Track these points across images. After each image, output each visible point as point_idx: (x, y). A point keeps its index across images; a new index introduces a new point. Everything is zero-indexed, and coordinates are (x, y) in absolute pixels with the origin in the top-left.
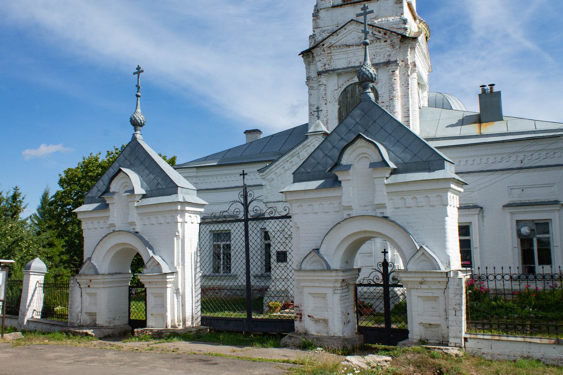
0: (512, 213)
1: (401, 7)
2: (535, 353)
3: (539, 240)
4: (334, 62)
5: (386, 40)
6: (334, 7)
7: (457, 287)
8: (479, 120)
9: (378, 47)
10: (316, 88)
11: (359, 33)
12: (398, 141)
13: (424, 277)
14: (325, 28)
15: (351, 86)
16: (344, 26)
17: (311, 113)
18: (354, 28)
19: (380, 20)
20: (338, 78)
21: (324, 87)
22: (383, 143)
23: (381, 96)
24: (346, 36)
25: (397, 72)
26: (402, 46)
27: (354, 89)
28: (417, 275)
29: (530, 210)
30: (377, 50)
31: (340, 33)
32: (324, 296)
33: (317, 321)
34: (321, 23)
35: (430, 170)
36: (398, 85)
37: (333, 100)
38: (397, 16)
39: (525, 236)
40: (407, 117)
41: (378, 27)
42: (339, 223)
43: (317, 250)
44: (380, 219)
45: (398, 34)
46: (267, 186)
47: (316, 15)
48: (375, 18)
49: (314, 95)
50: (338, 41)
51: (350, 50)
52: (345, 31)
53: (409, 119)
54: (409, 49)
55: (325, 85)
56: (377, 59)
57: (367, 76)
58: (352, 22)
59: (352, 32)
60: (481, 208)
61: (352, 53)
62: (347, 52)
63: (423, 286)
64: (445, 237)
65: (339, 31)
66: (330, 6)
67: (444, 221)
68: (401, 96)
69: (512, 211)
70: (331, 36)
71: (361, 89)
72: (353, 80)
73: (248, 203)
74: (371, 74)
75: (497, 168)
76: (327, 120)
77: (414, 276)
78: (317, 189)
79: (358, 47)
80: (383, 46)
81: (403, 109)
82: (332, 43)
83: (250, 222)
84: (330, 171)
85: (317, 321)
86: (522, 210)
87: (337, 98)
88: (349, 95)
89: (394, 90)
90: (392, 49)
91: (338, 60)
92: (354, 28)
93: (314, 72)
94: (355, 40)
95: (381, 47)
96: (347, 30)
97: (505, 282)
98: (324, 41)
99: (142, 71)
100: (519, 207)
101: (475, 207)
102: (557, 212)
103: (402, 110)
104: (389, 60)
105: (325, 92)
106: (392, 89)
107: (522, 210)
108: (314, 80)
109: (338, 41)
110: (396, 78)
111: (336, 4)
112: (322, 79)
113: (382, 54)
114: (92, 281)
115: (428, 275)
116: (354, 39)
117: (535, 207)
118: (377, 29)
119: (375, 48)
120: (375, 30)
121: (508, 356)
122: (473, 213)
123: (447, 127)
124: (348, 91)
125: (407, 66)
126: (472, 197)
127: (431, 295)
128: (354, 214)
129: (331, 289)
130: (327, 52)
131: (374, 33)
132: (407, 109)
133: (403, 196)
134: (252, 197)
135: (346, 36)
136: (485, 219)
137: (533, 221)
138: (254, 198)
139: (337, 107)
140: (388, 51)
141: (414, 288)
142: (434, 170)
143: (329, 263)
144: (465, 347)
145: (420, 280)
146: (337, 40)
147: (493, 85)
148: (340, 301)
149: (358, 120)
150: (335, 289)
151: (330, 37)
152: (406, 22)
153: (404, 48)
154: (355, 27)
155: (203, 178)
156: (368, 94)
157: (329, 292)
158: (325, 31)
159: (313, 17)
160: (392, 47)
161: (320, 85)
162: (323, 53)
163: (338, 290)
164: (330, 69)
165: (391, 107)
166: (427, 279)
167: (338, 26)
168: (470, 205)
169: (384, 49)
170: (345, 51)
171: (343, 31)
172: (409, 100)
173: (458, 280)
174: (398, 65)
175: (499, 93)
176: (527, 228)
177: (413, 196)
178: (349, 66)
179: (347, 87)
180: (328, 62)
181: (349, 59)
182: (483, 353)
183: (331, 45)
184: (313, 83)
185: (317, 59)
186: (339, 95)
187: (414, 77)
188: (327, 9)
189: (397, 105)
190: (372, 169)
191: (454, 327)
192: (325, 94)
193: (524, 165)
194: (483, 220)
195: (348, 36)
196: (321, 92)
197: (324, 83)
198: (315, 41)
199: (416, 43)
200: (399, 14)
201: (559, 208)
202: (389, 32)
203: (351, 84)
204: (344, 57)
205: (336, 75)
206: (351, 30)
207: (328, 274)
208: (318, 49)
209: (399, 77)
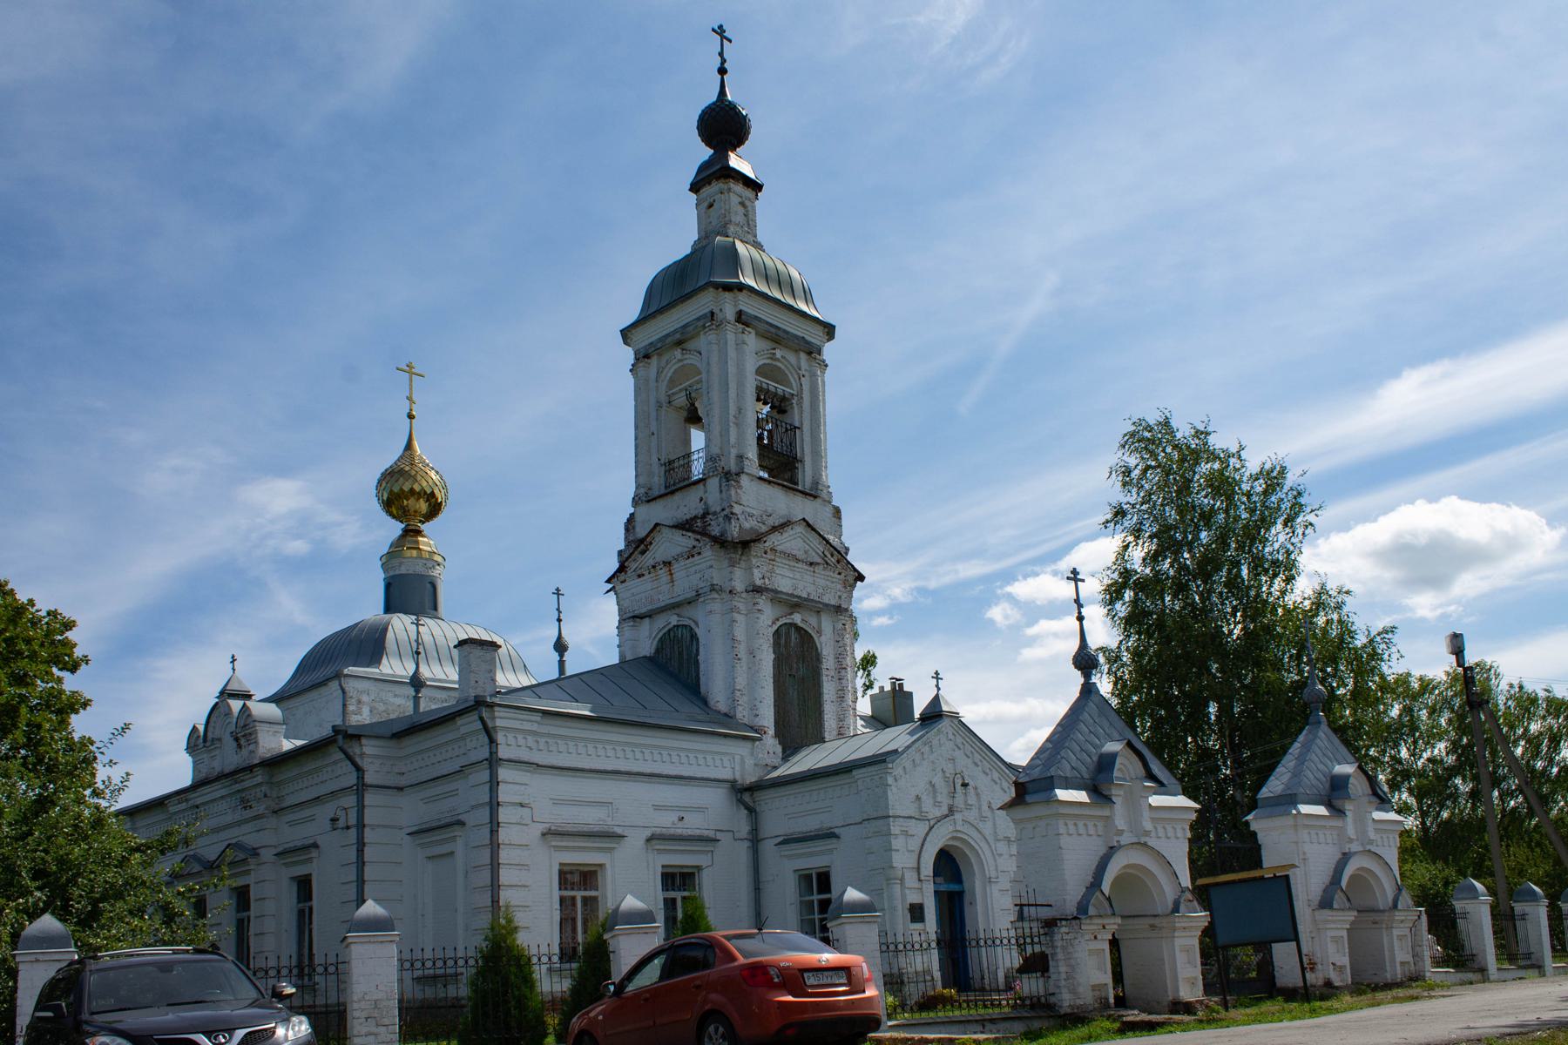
27: (789, 632)
46: (893, 787)
91: (780, 577)
97: (1012, 947)
114: (1107, 927)
154: (801, 530)
178: (795, 593)
184: (740, 602)
203: (785, 624)
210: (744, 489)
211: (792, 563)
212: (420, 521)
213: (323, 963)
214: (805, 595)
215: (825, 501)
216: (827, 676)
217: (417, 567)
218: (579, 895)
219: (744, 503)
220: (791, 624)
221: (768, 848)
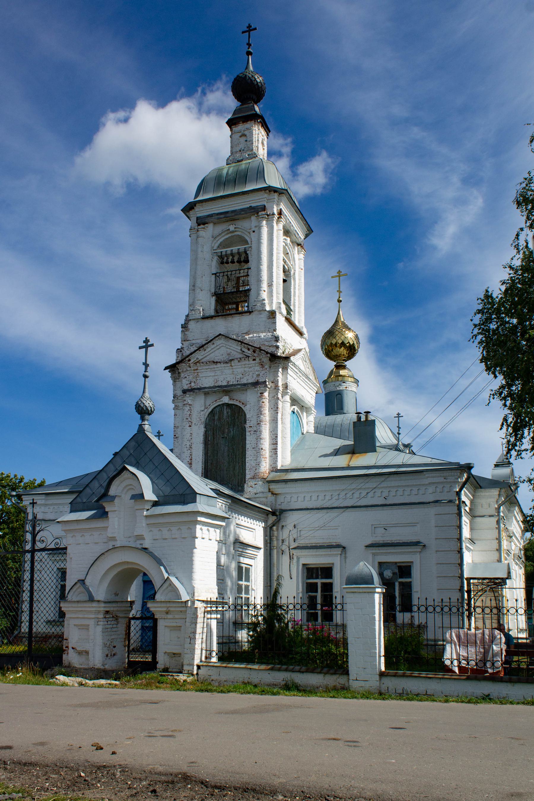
0: (374, 554)
1: (274, 323)
2: (254, 679)
3: (401, 584)
4: (200, 379)
5: (254, 358)
6: (204, 318)
7: (193, 616)
8: (352, 451)
9: (247, 366)
10: (181, 408)
11: (227, 349)
12: (162, 474)
13: (168, 607)
14: (194, 342)
15: (219, 408)
16: (212, 340)
17: (175, 436)
18: (222, 343)
19: (251, 336)
20: (205, 398)
21: (188, 408)
22: (150, 475)
23: (248, 420)
24: (215, 351)
25: (266, 394)
26: (272, 365)
27: (222, 410)
28: (163, 605)
29: (392, 551)
30: (246, 369)
31: (207, 347)
32: (86, 627)
33: (80, 653)
34: (190, 335)
35: (184, 503)
36: (267, 409)
37: (199, 422)
38: (270, 332)
39: (387, 580)
40: (275, 444)
41: (247, 344)
42: (103, 554)
43: (83, 581)
44: (139, 550)
45: (267, 353)
47: (185, 327)
48: (246, 333)
49: (179, 415)
50: (206, 357)
51: (217, 368)
52: (213, 346)
53: (277, 447)
54: (280, 370)
55: (190, 405)
56: (245, 378)
57: (142, 408)
58: (220, 336)
59: (220, 347)
60: (344, 548)
61: (220, 371)
62: (214, 369)
63: (169, 616)
64: (192, 568)
65: (207, 345)
66: (200, 317)
67: (192, 553)
68: (270, 420)
69: (374, 551)
70: (198, 351)
71: (229, 410)
72: (221, 401)
73: (37, 532)
74: (146, 406)
75: (362, 505)
76: (191, 444)
77: (160, 606)
78: (87, 519)
79: (225, 365)
80: (251, 365)
81: (272, 436)
82: (199, 359)
83: (36, 553)
84: (97, 501)
85: (80, 653)
86: (384, 551)
87: (203, 420)
88: (216, 418)
89: (261, 414)
90: (261, 369)
91: (204, 378)
92: (222, 343)
93: (179, 389)
94: (224, 356)
95: (250, 366)
96: (215, 345)
98: (191, 356)
99: (152, 345)
100: (380, 548)
101: (338, 546)
102: (418, 554)
103: (270, 437)
104: (258, 380)
105: (189, 413)
106: (259, 413)
107: (384, 551)
108: (179, 398)
109: (206, 357)
110: (264, 400)
111: (207, 315)
112: (186, 398)
113: (251, 373)
115: (172, 605)
116: (223, 355)
117: (396, 548)
118: (246, 345)
119: (243, 366)
120: (244, 347)
121: (232, 682)
122: (335, 553)
123: (320, 457)
124: (215, 412)
125: (276, 387)
126: (336, 535)
127: (175, 624)
128: (118, 544)
129: (93, 620)
130: (193, 369)
131: (244, 349)
132: (275, 435)
133: (161, 528)
134: (40, 527)
135: (215, 351)
136: (347, 560)
137: (396, 563)
138: (42, 528)
139: (202, 430)
140: (257, 371)
141: (162, 618)
142: (187, 504)
143: (93, 594)
144: (197, 674)
145: (165, 609)
146: (204, 356)
147: (370, 412)
148: (103, 632)
149: (132, 452)
150: (98, 620)
151: (196, 352)
152: (277, 339)
153: (274, 368)
154: (223, 342)
155: (52, 507)
156: (143, 426)
157: (91, 623)
158: (193, 344)
159: (182, 328)
160: (261, 366)
161: (184, 405)
162: (189, 369)
163: (101, 621)
164: (196, 387)
165: (258, 433)
166: (171, 609)
167: (207, 340)
168: (333, 544)
169: (253, 368)
170: (212, 368)
171: (211, 346)
172: (277, 425)
173: (194, 609)
174: (266, 386)
175: (373, 422)
176: (389, 571)
177: (168, 528)
178: (217, 385)
179: (215, 408)
180: (194, 380)
181: (216, 377)
182: (212, 680)
183: (198, 360)
185: (182, 375)
186: (206, 417)
187: (285, 400)
188: (197, 320)
189: (264, 431)
190: (133, 500)
191: (188, 655)
192: (190, 415)
193: (388, 502)
194: (345, 560)
195: (216, 352)
196: (186, 413)
197: (190, 403)
198: (182, 355)
199: (289, 362)
200: (271, 330)
201: (420, 550)
202: (258, 350)
203: (219, 405)
204: (211, 375)
205: (203, 394)
206: (219, 345)
207: (89, 604)
208: (184, 364)
209: (268, 400)
210: (190, 330)
211: (212, 366)
212: (344, 360)
213: (428, 614)
214: (225, 383)
215: (260, 311)
216: (250, 431)
217: (330, 388)
218: (319, 582)
219: (190, 339)
220: (223, 404)
221: (290, 550)
